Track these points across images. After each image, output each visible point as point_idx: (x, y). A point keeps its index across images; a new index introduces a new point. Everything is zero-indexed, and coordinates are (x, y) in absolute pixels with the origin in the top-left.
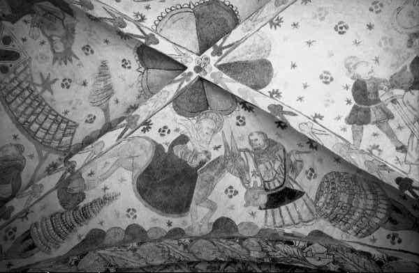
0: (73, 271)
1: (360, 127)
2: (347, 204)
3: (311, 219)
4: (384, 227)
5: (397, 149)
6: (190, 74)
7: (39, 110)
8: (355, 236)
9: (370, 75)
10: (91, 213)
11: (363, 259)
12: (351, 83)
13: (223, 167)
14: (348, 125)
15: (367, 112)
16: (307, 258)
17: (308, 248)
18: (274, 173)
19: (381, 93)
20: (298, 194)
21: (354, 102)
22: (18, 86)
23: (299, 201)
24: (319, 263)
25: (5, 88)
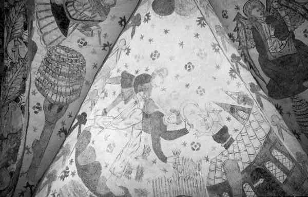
2: (60, 72)
3: (46, 42)
5: (105, 109)
8: (36, 78)
9: (154, 86)
11: (18, 87)
12: (150, 73)
14: (121, 73)
15: (130, 85)
16: (13, 40)
18: (81, 11)
19: (142, 93)
20: (65, 31)
21: (136, 75)
23: (59, 32)
24: (10, 51)
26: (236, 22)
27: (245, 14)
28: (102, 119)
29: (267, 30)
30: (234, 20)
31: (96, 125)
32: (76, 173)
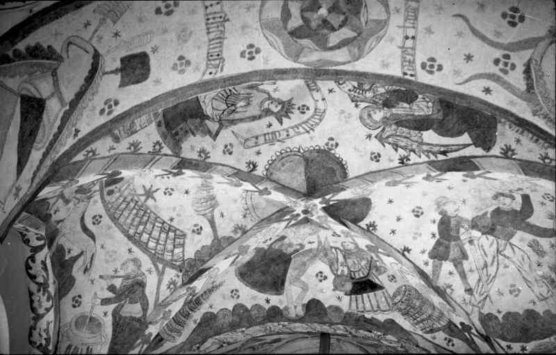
0: (196, 352)
1: (440, 262)
4: (444, 331)
5: (465, 291)
6: (298, 215)
7: (145, 218)
10: (202, 300)
12: (438, 217)
13: (315, 256)
15: (447, 247)
19: (462, 230)
22: (123, 201)
23: (379, 292)
25: (112, 206)
26: (386, 144)
27: (379, 127)
28: (476, 296)
29: (402, 109)
30: (384, 146)
31: (480, 305)
32: (525, 345)
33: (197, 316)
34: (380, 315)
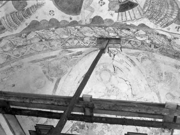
4: (175, 23)
10: (32, 12)
16: (136, 37)
17: (137, 32)
20: (135, 5)
23: (135, 9)
33: (28, 21)
34: (135, 22)
